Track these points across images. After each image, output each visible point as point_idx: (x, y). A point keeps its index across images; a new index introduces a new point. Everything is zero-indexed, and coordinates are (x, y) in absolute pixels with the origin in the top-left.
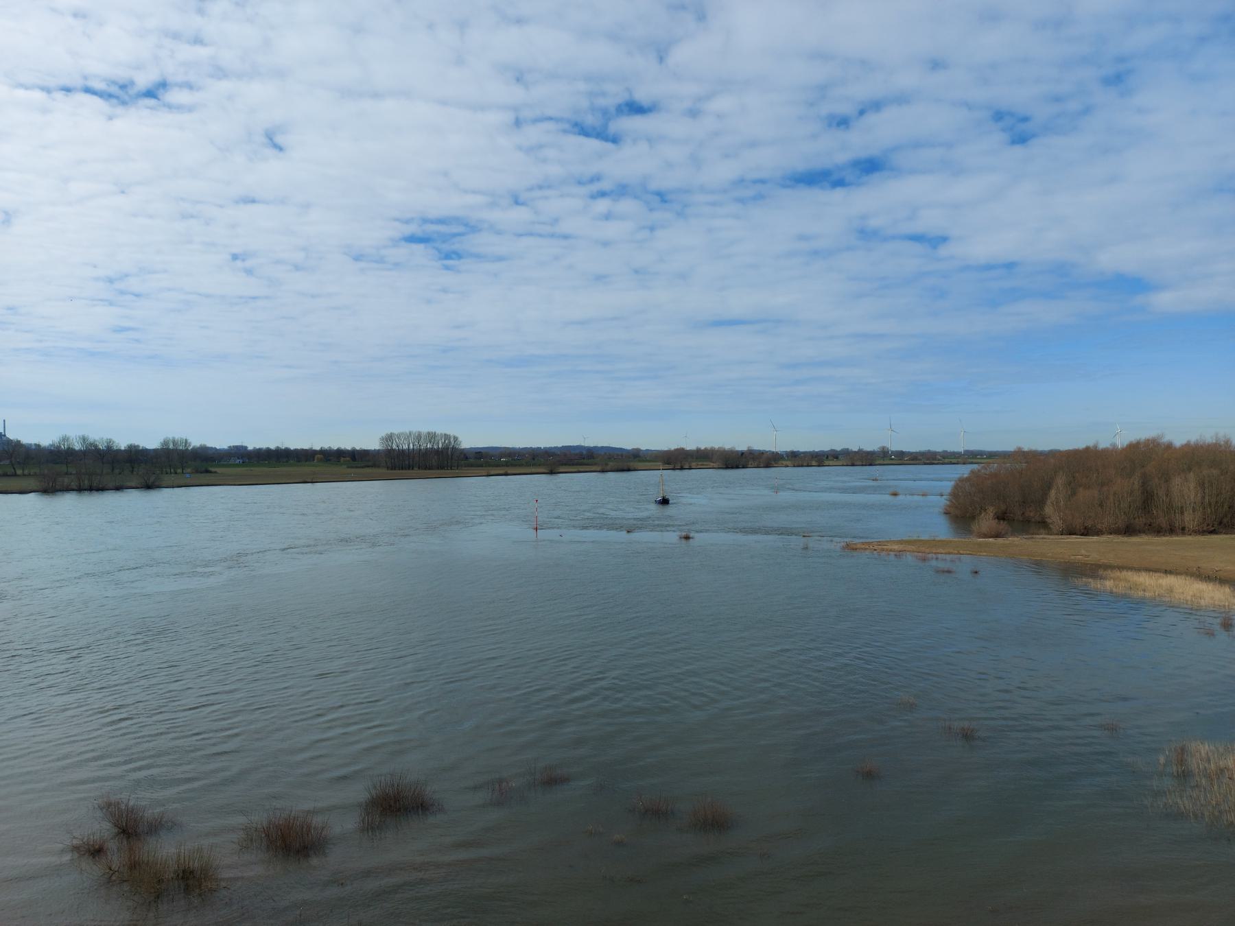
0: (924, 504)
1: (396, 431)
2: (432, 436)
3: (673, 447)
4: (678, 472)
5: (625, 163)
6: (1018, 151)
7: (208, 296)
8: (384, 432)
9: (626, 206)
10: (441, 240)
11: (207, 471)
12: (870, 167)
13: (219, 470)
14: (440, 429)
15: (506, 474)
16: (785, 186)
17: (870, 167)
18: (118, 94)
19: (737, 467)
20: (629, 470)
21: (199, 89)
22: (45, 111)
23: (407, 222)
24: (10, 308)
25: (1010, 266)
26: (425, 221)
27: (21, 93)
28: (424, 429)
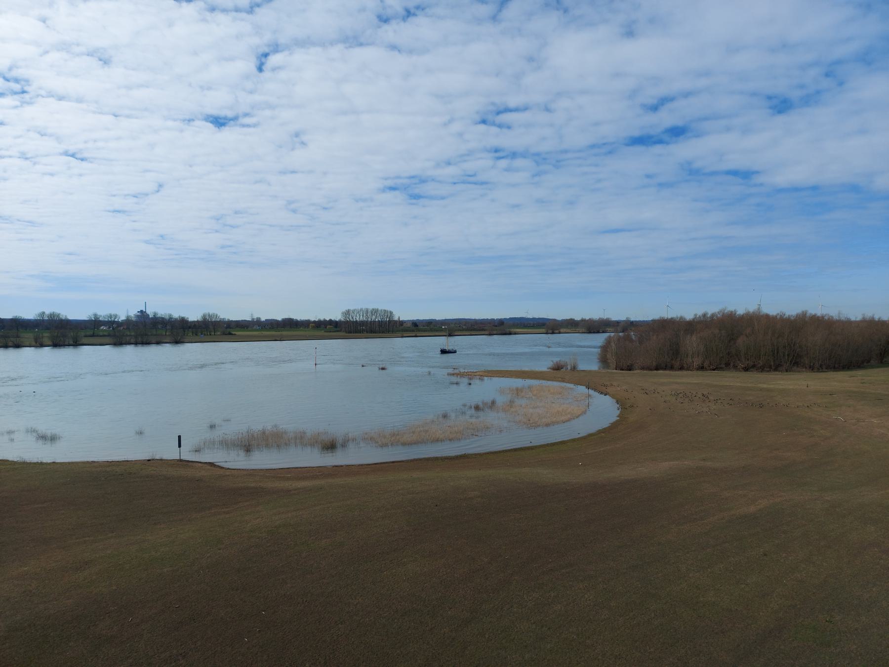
0: (586, 351)
1: (352, 308)
2: (375, 311)
3: (657, 317)
4: (549, 335)
5: (509, 140)
6: (781, 119)
7: (271, 226)
8: (344, 309)
9: (519, 163)
10: (411, 189)
11: (230, 334)
12: (677, 132)
13: (237, 333)
14: (381, 307)
15: (416, 336)
16: (627, 145)
17: (677, 132)
18: (219, 122)
19: (598, 332)
20: (510, 334)
21: (252, 116)
22: (181, 131)
23: (386, 179)
24: (162, 236)
25: (815, 188)
26: (398, 177)
27: (170, 123)
28: (371, 307)
